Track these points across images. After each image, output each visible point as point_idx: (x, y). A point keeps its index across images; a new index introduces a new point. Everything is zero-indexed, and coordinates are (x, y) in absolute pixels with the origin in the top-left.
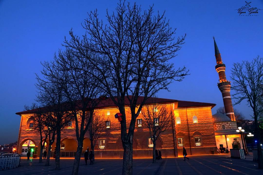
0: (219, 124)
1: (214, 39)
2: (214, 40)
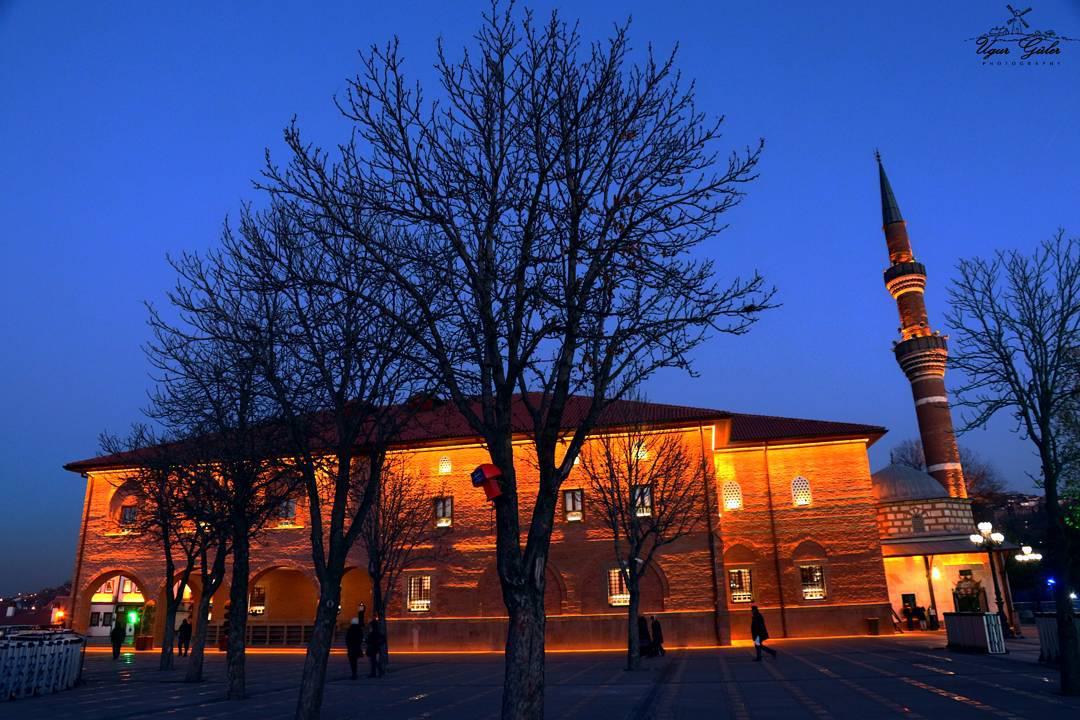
0: (899, 512)
1: (879, 160)
2: (880, 166)
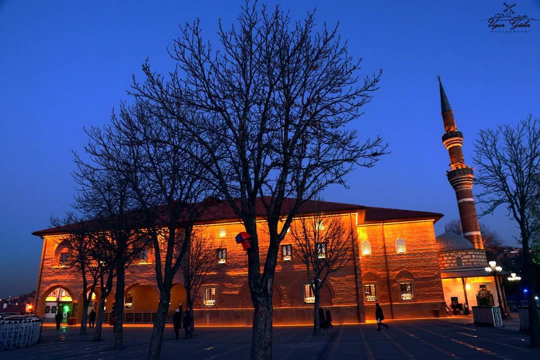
0: (450, 256)
1: (439, 80)
2: (440, 83)
